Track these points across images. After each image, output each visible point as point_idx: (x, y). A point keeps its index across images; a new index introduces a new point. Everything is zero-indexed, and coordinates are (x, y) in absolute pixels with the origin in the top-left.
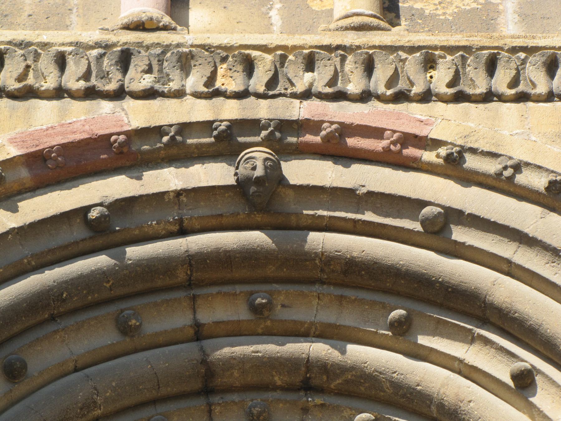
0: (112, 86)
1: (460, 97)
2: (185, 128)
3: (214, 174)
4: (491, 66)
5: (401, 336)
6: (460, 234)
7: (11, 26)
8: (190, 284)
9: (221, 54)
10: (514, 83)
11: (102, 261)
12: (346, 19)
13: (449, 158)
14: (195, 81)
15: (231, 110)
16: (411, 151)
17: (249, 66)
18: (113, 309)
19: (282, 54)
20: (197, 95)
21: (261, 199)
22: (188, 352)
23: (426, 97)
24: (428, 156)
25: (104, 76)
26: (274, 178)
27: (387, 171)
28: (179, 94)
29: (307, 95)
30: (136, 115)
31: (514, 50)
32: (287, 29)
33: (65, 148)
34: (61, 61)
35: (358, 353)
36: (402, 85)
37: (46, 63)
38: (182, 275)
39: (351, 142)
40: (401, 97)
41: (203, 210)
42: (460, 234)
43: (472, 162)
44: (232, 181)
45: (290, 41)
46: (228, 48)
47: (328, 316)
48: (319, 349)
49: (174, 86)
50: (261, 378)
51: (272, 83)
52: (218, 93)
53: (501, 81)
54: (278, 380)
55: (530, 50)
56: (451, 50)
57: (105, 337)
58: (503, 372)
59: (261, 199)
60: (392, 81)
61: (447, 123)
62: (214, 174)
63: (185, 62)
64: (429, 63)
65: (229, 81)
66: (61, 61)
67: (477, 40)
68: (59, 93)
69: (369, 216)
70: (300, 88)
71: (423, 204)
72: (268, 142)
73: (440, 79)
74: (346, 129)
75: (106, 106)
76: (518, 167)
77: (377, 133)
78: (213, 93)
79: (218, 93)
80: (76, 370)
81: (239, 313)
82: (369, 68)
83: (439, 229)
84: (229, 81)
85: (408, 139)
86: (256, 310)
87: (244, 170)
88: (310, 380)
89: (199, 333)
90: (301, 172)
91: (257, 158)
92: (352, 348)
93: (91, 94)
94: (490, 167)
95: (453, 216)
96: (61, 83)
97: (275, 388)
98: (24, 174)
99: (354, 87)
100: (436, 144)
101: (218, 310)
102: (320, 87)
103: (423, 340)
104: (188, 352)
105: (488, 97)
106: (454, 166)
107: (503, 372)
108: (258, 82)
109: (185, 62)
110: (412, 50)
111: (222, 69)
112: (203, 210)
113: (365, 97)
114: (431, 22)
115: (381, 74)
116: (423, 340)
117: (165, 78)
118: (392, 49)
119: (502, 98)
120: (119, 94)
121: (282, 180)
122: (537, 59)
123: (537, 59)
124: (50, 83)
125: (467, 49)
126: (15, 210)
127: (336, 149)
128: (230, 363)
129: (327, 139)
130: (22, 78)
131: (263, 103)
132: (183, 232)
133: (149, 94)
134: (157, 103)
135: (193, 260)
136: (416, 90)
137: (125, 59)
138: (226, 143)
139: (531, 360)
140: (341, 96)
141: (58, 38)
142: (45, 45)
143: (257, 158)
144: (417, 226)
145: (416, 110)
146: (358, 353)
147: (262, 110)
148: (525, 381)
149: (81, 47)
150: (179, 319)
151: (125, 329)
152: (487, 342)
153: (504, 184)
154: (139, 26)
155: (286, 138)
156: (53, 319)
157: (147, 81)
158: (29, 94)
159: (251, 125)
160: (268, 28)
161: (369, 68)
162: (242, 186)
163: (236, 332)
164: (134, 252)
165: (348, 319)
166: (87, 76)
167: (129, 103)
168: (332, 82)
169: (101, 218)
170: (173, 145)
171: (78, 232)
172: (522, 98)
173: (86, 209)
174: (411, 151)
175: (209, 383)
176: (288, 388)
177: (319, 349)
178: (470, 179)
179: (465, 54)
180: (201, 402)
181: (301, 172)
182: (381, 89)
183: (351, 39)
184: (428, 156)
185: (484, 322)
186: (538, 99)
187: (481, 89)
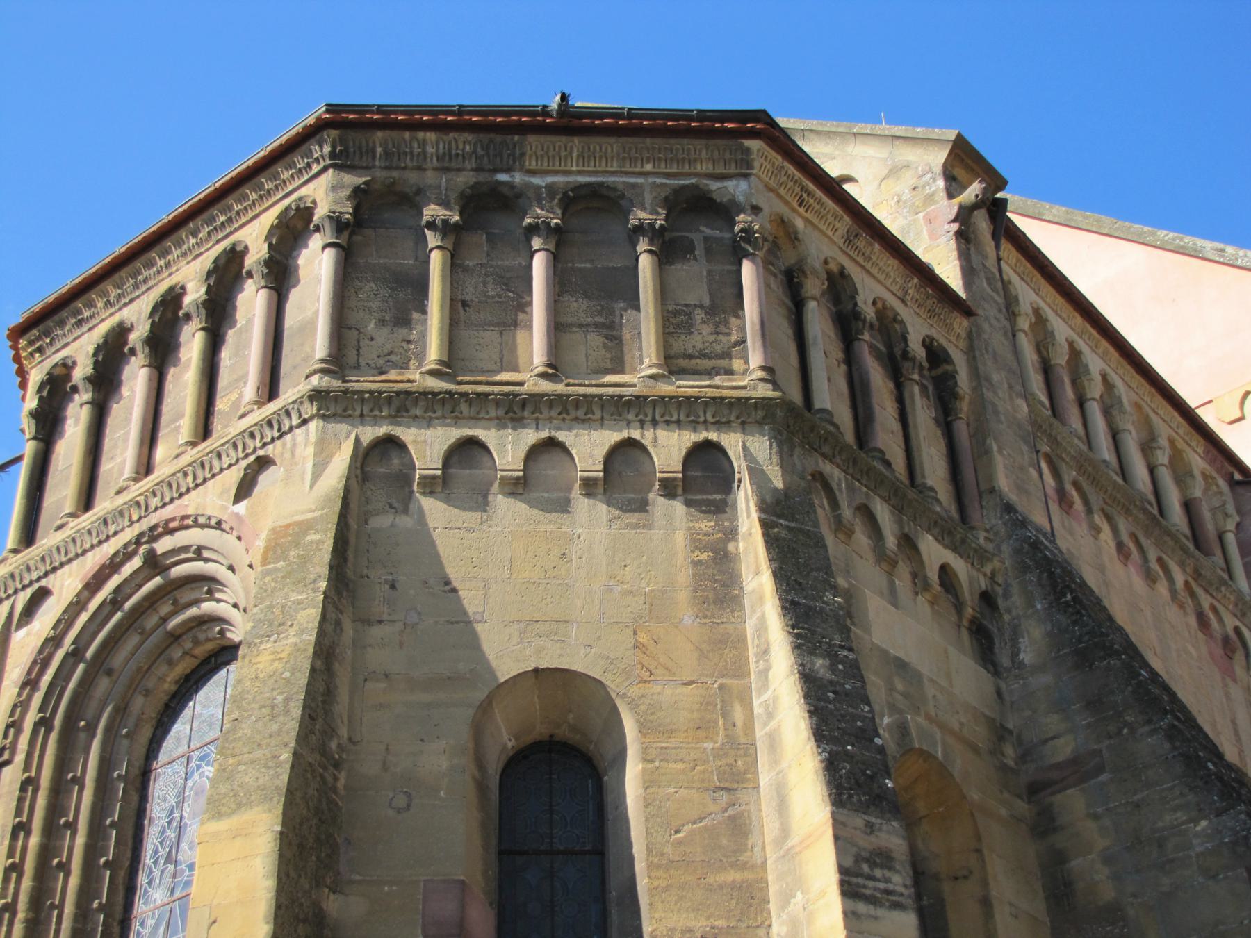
21: (154, 564)
90: (162, 546)
101: (165, 609)
103: (460, 378)
112: (141, 576)
132: (140, 586)
145: (169, 508)
155: (153, 534)
156: (116, 643)
158: (84, 552)
163: (174, 613)
170: (113, 565)
175: (174, 637)
181: (162, 546)
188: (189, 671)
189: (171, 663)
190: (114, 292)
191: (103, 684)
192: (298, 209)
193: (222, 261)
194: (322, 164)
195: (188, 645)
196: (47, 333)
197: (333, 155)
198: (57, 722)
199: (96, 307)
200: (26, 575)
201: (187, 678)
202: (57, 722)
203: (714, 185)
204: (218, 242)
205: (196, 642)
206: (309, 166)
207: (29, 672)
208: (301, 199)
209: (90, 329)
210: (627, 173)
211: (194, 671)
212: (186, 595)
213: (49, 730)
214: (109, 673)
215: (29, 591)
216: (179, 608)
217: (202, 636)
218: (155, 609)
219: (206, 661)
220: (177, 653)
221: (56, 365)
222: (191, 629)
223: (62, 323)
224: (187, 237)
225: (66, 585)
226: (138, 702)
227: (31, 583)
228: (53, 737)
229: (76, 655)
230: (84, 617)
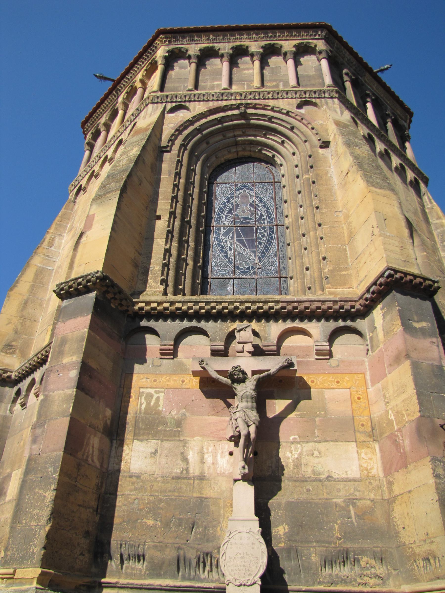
0: (221, 99)
1: (273, 99)
2: (232, 105)
3: (236, 112)
4: (278, 93)
5: (265, 136)
6: (273, 120)
7: (206, 90)
8: (233, 129)
9: (237, 93)
10: (282, 96)
11: (220, 126)
12: (283, 119)
13: (272, 108)
14: (233, 98)
15: (239, 102)
16: (266, 107)
17: (241, 95)
18: (222, 133)
19: (246, 93)
20: (234, 100)
21: (244, 115)
22: (233, 139)
23: (268, 99)
24: (269, 108)
25: (219, 97)
26: (245, 112)
27: (262, 111)
28: (231, 100)
29: (250, 99)
30: (224, 103)
31: (281, 91)
32: (248, 89)
33: (214, 109)
34: (213, 95)
35: (259, 138)
36: (264, 97)
37: (211, 96)
38: (232, 128)
39: (257, 106)
40: (264, 99)
41: (235, 118)
42: (273, 120)
43: (275, 109)
44: (239, 113)
45: (248, 91)
46: (238, 92)
47: (254, 133)
48: (253, 138)
49: (230, 98)
50: (244, 143)
51: (245, 97)
52: (237, 99)
53: (279, 96)
54: (247, 143)
55: (284, 91)
56: (272, 91)
57: (221, 137)
58: (280, 141)
59: (244, 115)
60: (263, 96)
61: (271, 103)
62: (236, 112)
63: (232, 95)
64: (269, 93)
65: (238, 97)
66: (213, 95)
67: (276, 89)
68: (213, 100)
69: (260, 118)
70: (249, 98)
71: (267, 115)
72: (244, 107)
73: (270, 96)
74: (256, 104)
75: (220, 102)
76: (282, 109)
77: (261, 105)
78: (236, 99)
79: (237, 99)
80: (217, 142)
81: (240, 133)
82: (259, 94)
83: (270, 119)
84: (238, 97)
85: (265, 106)
86: (243, 132)
87: (241, 111)
88: (252, 143)
89: (235, 136)
90: (249, 111)
91: (243, 109)
92: (257, 138)
93: (218, 100)
94: (278, 109)
95: (272, 117)
96: (262, 68)
97: (246, 144)
98: (208, 113)
99: (257, 98)
100: (269, 106)
101: (237, 133)
102: (252, 98)
103: (268, 136)
104: (233, 139)
105: (278, 98)
106: (272, 110)
107: (280, 141)
108: (243, 97)
109: (232, 95)
110: (266, 91)
111: (237, 96)
112: (235, 118)
113: (259, 99)
114: (269, 87)
115: (261, 95)
116: (268, 136)
117: (228, 97)
118: (263, 91)
119: (280, 99)
120: (222, 100)
121: (247, 112)
122: (285, 92)
123: (285, 92)
124: (211, 99)
125: (274, 91)
126: (207, 119)
127: (255, 107)
128: (240, 140)
129: (253, 106)
130: (207, 98)
131: (244, 101)
132: (232, 121)
133: (226, 100)
134: (227, 101)
135: (234, 125)
136: (267, 98)
137: (222, 95)
138: (238, 107)
139: (284, 139)
140: (255, 99)
141: (212, 92)
142: (210, 93)
143: (243, 109)
144: (267, 119)
145: (267, 101)
146: (259, 138)
147: (243, 102)
148: (283, 142)
149: (216, 93)
150: (231, 134)
151: (224, 136)
152: (277, 136)
153: (280, 112)
154: (225, 89)
155: (247, 106)
156: (213, 135)
157: (226, 98)
158: (208, 101)
159: (241, 104)
160: (244, 89)
161: (259, 94)
162: (241, 113)
163: (241, 136)
164: (225, 124)
165: (257, 133)
166: (217, 97)
167: (224, 102)
168: (254, 97)
169: (220, 119)
170: (230, 108)
171: (216, 122)
172: (283, 98)
173: (217, 118)
174: (266, 107)
175: (237, 144)
176: (248, 144)
177: (253, 138)
178: (275, 111)
179: (403, 164)
180: (235, 147)
181: (249, 111)
182: (261, 98)
183: (257, 90)
184: (269, 108)
185: (277, 133)
186: (285, 99)
187: (276, 97)
188: (231, 159)
189: (229, 152)
190: (211, 37)
191: (204, 146)
192: (306, 45)
193: (267, 46)
194: (320, 37)
195: (240, 149)
196: (175, 38)
197: (325, 36)
198: (189, 147)
199: (202, 38)
200: (174, 98)
201: (229, 161)
202: (189, 147)
203: (400, 119)
204: (267, 40)
205: (244, 150)
206: (315, 35)
207: (180, 127)
208: (309, 43)
209: (196, 44)
210: (383, 99)
211: (233, 160)
212: (251, 132)
213: (185, 149)
214: (208, 143)
215: (174, 104)
216: (244, 135)
217: (248, 148)
218: (234, 131)
219: (241, 158)
220: (234, 150)
221: (177, 48)
222: (244, 144)
223: (183, 38)
224: (253, 34)
225: (199, 108)
226: (213, 159)
227: (176, 102)
228: (186, 153)
229: (198, 131)
230: (204, 121)
